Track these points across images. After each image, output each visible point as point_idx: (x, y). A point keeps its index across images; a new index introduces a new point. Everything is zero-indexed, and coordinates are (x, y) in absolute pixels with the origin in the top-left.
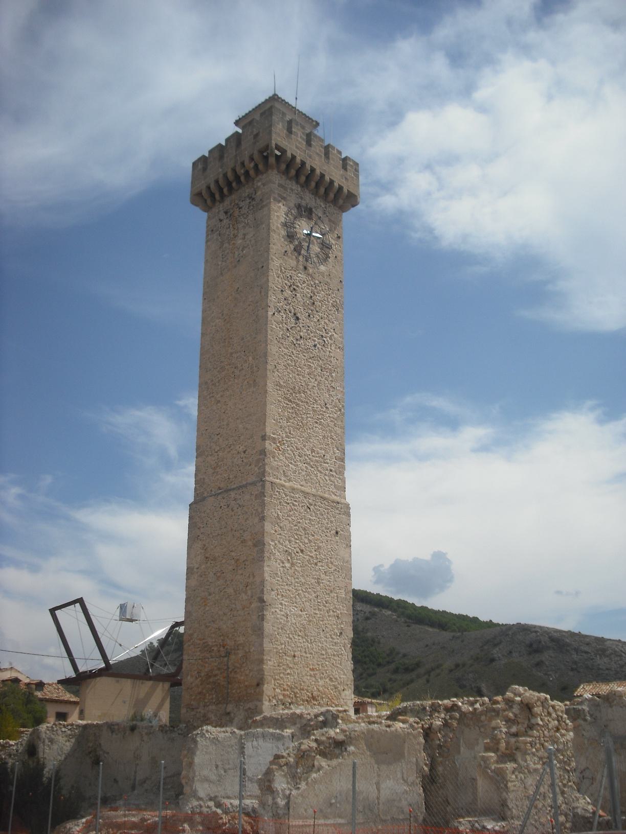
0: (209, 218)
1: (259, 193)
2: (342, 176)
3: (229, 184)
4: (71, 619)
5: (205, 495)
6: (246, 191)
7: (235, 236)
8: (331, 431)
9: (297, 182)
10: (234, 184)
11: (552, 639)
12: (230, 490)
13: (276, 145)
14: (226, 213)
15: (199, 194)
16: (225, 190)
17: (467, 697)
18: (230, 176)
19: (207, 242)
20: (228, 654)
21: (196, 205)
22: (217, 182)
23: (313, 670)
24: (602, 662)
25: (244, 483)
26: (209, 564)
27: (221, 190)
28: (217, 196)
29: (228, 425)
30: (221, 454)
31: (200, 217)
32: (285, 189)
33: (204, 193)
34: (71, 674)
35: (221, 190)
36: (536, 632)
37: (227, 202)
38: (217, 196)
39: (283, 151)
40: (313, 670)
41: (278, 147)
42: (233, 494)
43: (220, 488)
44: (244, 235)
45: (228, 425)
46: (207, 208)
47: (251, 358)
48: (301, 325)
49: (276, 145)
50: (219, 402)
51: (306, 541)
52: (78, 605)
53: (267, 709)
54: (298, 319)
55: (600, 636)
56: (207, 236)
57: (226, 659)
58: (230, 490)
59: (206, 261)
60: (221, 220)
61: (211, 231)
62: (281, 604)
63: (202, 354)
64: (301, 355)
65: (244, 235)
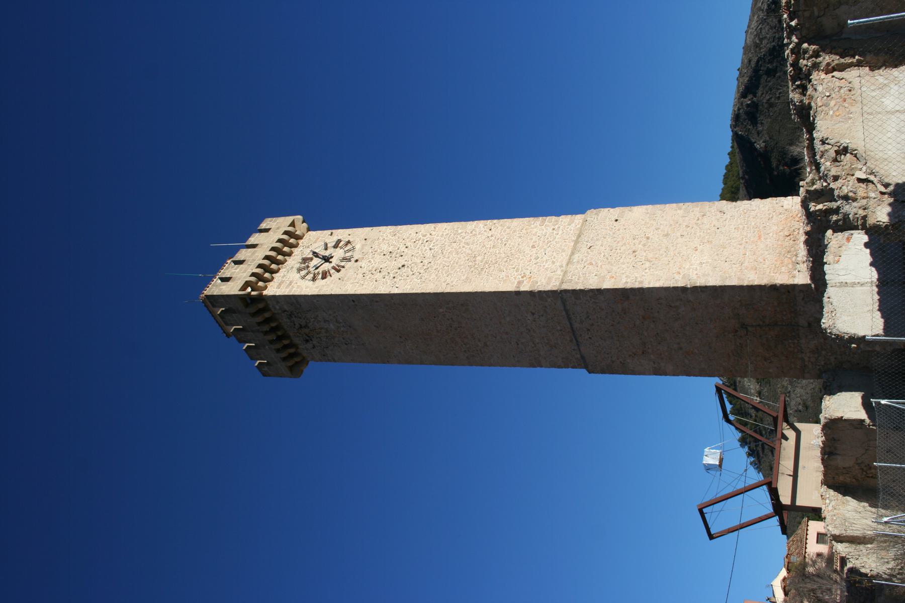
0: (313, 359)
1: (286, 307)
2: (275, 232)
3: (280, 338)
4: (719, 519)
5: (579, 356)
6: (284, 321)
7: (327, 331)
8: (515, 231)
9: (277, 271)
10: (279, 333)
11: (744, 95)
12: (572, 328)
13: (240, 290)
14: (307, 341)
15: (291, 368)
16: (286, 342)
17: (791, 115)
18: (272, 337)
19: (335, 361)
20: (744, 326)
21: (302, 371)
22: (278, 351)
23: (760, 237)
24: (766, 45)
25: (564, 313)
26: (650, 351)
27: (285, 347)
28: (292, 351)
29: (507, 333)
30: (537, 341)
31: (313, 369)
32: (282, 282)
33: (290, 363)
34: (775, 520)
35: (285, 347)
36: (739, 109)
37: (296, 341)
38: (292, 351)
39: (247, 284)
40: (760, 237)
41: (244, 288)
42: (576, 325)
43: (571, 341)
44: (325, 321)
45: (507, 333)
46: (304, 362)
47: (441, 310)
48: (410, 262)
49: (240, 290)
50: (485, 344)
51: (624, 248)
52: (705, 510)
53: (802, 278)
54: (403, 266)
55: (742, 51)
56: (329, 360)
57: (750, 329)
58: (572, 328)
59: (353, 361)
60: (314, 347)
61: (324, 357)
62: (689, 269)
63: (441, 364)
64: (439, 262)
65: (325, 321)
